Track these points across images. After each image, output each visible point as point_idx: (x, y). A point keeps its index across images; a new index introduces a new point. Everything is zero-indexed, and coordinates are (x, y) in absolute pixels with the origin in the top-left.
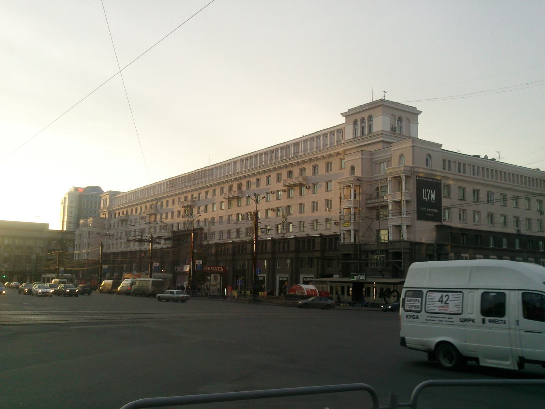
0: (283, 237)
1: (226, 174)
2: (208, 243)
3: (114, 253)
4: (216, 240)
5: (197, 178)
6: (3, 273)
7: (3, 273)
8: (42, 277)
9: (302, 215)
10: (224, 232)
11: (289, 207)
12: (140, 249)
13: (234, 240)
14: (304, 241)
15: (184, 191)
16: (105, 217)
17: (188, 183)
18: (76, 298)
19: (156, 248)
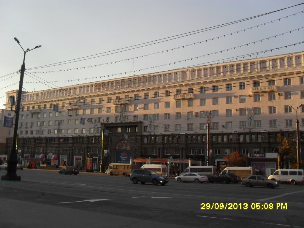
0: (250, 131)
1: (178, 80)
2: (151, 134)
4: (160, 131)
9: (273, 115)
11: (49, 122)
12: (58, 136)
13: (34, 136)
15: (196, 82)
17: (120, 86)
18: (76, 176)
19: (64, 137)
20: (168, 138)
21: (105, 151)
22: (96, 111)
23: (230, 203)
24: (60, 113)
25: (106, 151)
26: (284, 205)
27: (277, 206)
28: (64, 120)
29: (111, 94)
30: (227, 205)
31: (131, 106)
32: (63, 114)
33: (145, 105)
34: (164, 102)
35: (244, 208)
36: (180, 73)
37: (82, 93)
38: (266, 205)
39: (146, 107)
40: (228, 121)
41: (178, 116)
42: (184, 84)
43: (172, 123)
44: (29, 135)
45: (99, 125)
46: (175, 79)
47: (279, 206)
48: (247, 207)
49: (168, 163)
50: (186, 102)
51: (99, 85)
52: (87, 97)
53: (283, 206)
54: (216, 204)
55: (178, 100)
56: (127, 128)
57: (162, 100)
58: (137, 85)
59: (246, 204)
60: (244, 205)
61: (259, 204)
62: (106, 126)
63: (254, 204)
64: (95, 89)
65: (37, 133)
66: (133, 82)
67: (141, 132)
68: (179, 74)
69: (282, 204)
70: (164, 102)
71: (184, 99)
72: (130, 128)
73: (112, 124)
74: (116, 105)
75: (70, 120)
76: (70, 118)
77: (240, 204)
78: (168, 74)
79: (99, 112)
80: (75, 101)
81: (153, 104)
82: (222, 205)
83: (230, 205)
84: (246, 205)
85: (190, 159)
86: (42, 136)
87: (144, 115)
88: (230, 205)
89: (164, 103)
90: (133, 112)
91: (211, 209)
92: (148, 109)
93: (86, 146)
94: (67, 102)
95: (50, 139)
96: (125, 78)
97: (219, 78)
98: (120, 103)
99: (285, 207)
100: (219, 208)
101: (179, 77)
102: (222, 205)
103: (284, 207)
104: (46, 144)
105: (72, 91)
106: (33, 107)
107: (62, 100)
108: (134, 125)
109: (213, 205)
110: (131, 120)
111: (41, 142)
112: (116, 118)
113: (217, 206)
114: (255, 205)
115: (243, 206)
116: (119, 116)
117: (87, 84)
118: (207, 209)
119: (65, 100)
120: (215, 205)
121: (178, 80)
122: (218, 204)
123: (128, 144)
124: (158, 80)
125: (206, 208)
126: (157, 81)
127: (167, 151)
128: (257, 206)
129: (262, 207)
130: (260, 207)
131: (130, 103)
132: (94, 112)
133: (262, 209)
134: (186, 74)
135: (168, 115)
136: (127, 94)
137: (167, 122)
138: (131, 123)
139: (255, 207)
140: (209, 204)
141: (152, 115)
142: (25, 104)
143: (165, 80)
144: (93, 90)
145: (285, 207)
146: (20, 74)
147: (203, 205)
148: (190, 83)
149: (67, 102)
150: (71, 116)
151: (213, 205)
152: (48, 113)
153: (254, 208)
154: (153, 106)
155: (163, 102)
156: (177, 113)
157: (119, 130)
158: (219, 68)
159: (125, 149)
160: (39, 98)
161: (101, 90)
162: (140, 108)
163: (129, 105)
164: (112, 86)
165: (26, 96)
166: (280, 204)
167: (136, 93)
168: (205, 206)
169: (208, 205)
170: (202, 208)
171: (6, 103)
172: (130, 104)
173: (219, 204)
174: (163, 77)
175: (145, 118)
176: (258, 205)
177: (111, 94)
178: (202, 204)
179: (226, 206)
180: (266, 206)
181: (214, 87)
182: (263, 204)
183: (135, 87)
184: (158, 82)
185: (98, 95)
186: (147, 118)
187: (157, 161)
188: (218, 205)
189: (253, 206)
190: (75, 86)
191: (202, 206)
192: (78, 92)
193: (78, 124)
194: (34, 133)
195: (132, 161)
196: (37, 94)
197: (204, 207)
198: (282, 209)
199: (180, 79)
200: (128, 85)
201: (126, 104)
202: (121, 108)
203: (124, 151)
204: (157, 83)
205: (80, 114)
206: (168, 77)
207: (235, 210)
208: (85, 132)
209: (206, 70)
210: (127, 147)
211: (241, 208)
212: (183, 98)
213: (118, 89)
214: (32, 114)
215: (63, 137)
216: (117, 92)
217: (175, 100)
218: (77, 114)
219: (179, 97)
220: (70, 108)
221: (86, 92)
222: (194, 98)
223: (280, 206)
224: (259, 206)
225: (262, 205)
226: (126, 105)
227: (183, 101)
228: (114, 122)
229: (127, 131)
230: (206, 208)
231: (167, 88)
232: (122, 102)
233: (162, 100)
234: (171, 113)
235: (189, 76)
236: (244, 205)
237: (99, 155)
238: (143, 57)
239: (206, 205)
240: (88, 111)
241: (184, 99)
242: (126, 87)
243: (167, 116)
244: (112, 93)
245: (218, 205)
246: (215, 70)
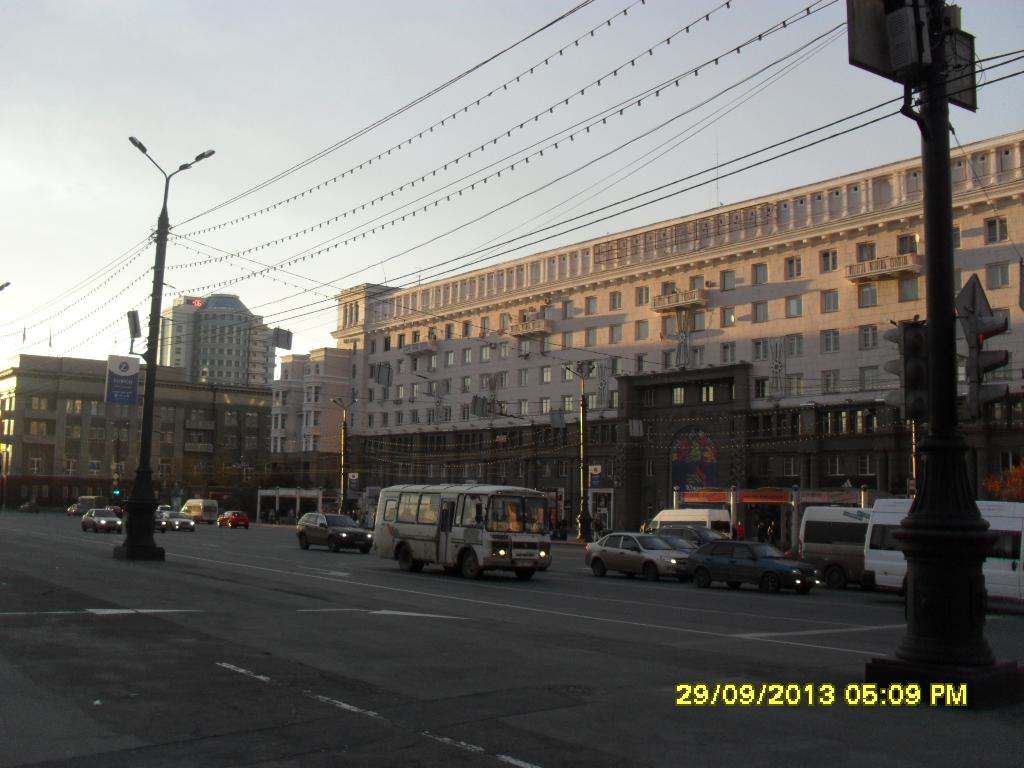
2: (778, 406)
3: (393, 438)
4: (806, 395)
5: (668, 241)
6: (115, 483)
7: (115, 483)
8: (259, 495)
10: (843, 375)
12: (491, 424)
14: (768, 418)
15: (967, 202)
16: (352, 348)
17: (675, 247)
19: (509, 426)
20: (837, 415)
21: (591, 469)
22: (602, 337)
23: (776, 683)
24: (494, 348)
25: (596, 470)
26: (957, 690)
27: (934, 695)
28: (505, 372)
29: (645, 276)
30: (764, 691)
31: (710, 313)
32: (505, 352)
33: (755, 305)
34: (817, 290)
35: (821, 700)
36: (867, 185)
37: (557, 278)
38: (793, 699)
39: (756, 317)
40: (865, 363)
41: (828, 341)
42: (880, 223)
43: (845, 362)
44: (412, 429)
45: (613, 384)
46: (850, 209)
47: (939, 695)
48: (832, 699)
49: (793, 503)
50: (893, 285)
51: (607, 251)
52: (571, 291)
53: (954, 695)
54: (727, 687)
55: (863, 282)
56: (704, 389)
57: (811, 286)
58: (727, 239)
59: (830, 687)
60: (821, 690)
61: (873, 686)
62: (636, 384)
63: (856, 687)
64: (597, 263)
65: (464, 416)
66: (712, 231)
67: (748, 400)
68: (863, 187)
69: (950, 687)
70: (819, 293)
71: (884, 277)
72: (711, 389)
73: (655, 375)
74: (665, 311)
75: (526, 370)
76: (523, 364)
77: (809, 688)
78: (826, 194)
79: (612, 340)
80: (537, 305)
81: (782, 301)
82: (747, 691)
83: (776, 691)
84: (827, 690)
85: (865, 490)
86: (445, 427)
87: (722, 344)
88: (776, 691)
89: (817, 295)
90: (719, 332)
91: (712, 703)
92: (765, 319)
93: (529, 454)
94: (514, 312)
95: (467, 436)
96: (686, 220)
97: (1005, 191)
98: (674, 304)
99: (962, 698)
100: (737, 701)
101: (863, 199)
102: (747, 691)
103: (957, 697)
104: (458, 450)
105: (527, 274)
106: (416, 335)
107: (497, 307)
108: (727, 377)
109: (718, 691)
110: (712, 359)
111: (435, 446)
112: (666, 355)
113: (730, 694)
114: (858, 692)
115: (817, 694)
116: (673, 350)
117: (569, 249)
118: (698, 703)
119: (507, 305)
120: (724, 692)
121: (863, 210)
122: (733, 687)
123: (709, 440)
124: (795, 216)
125: (693, 701)
126: (792, 221)
127: (834, 461)
128: (866, 694)
129: (881, 697)
130: (875, 696)
131: (707, 303)
132: (595, 339)
133: (884, 702)
134: (889, 187)
135: (870, 332)
136: (695, 273)
137: (831, 361)
138: (712, 370)
139: (859, 697)
140: (704, 687)
141: (781, 337)
142: (390, 326)
143: (816, 216)
144: (588, 268)
145: (962, 698)
146: (154, 245)
147: (684, 691)
148: (902, 217)
149: (514, 312)
150: (526, 356)
151: (718, 691)
152: (460, 352)
153: (856, 702)
154: (783, 307)
155: (815, 293)
156: (861, 327)
157: (679, 395)
158: (1007, 153)
159: (700, 458)
160: (432, 306)
161: (616, 265)
162: (740, 319)
163: (705, 310)
164: (635, 253)
165: (392, 300)
166: (942, 687)
167: (724, 267)
168: (692, 694)
169: (701, 691)
170: (680, 701)
171: (338, 327)
172: (708, 306)
173: (738, 689)
174: (809, 206)
175: (758, 351)
176: (868, 690)
177: (645, 276)
178: (679, 688)
179: (761, 695)
180: (896, 694)
181: (991, 223)
182: (887, 687)
183: (720, 245)
184: (796, 224)
185: (607, 284)
186: (765, 350)
187: (755, 497)
188: (736, 692)
189: (853, 694)
190: (535, 259)
191: (679, 695)
192: (544, 278)
193: (572, 380)
194: (423, 418)
195: (679, 499)
196: (426, 293)
197: (686, 696)
198: (948, 702)
199: (867, 206)
200: (675, 247)
201: (695, 306)
202: (680, 324)
203: (698, 468)
204: (791, 226)
205: (553, 348)
206: (826, 202)
207: (793, 706)
208: (571, 408)
209: (960, 164)
210: (706, 454)
211: (810, 702)
212: (880, 271)
213: (666, 256)
214: (414, 357)
215: (507, 429)
216: (663, 267)
217: (853, 281)
218: (546, 350)
219: (867, 269)
220: (522, 331)
221: (568, 275)
222: (918, 271)
223: (945, 695)
224: (872, 693)
225: (884, 692)
226: (693, 309)
227: (882, 282)
228: (659, 369)
229: (704, 400)
230: (695, 700)
231: (824, 242)
232: (682, 301)
233: (811, 286)
234: (844, 329)
235: (900, 193)
236: (821, 690)
237: (616, 483)
238: (402, 146)
239: (692, 690)
240: (578, 339)
241: (884, 277)
242: (691, 247)
243: (829, 338)
244: (649, 270)
245: (736, 692)
246: (992, 160)
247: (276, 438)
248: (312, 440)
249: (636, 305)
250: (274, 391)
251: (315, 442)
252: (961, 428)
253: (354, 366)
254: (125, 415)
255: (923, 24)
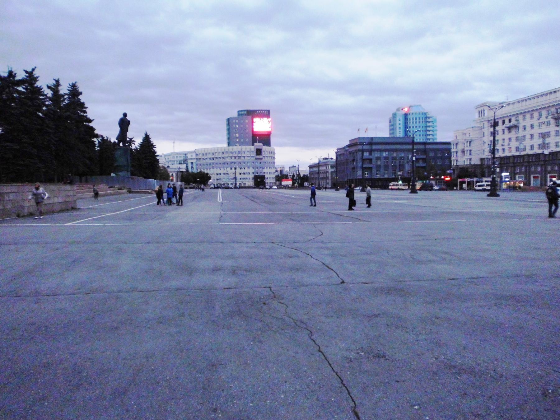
6: (399, 179)
7: (399, 179)
19: (551, 152)
86: (523, 153)
247: (454, 160)
248: (455, 161)
249: (533, 124)
250: (452, 143)
251: (470, 161)
252: (322, 170)
253: (484, 133)
254: (379, 155)
255: (398, 188)
